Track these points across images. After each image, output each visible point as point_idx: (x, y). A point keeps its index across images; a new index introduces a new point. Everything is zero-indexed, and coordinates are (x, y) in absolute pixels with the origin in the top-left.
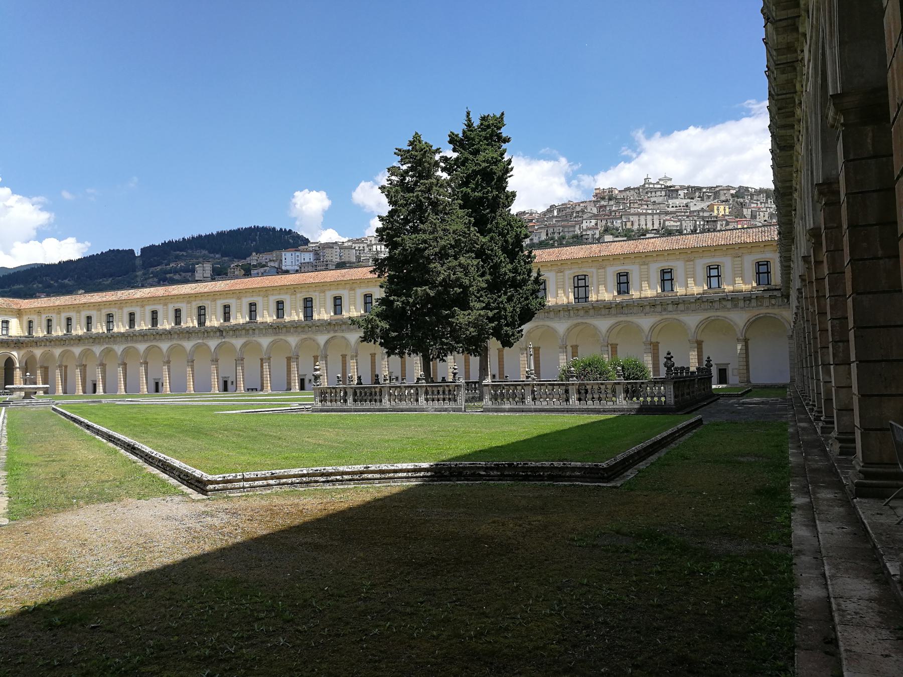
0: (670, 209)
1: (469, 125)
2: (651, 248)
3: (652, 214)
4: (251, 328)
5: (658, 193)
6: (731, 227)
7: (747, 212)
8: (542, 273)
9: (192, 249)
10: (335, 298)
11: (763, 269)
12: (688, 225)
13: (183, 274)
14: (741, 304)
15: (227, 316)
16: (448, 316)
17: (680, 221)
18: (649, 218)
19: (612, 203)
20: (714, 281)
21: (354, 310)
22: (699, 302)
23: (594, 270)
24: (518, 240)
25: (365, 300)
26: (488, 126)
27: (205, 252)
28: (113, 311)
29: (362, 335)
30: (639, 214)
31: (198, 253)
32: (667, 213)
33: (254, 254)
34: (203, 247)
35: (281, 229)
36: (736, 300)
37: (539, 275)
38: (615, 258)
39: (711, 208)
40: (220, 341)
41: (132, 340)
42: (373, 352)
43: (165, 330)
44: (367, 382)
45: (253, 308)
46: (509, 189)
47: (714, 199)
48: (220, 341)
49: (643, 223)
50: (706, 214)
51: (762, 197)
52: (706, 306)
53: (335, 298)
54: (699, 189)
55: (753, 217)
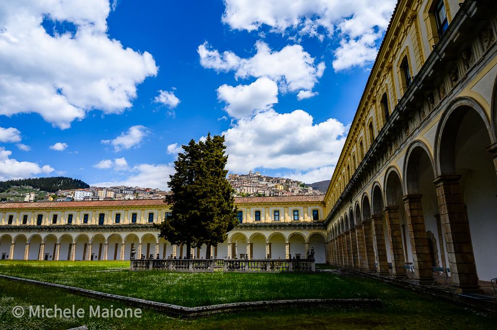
0: (260, 186)
1: (209, 139)
2: (270, 201)
3: (253, 187)
4: (69, 227)
5: (255, 178)
6: (284, 195)
7: (290, 189)
8: (238, 207)
9: (24, 185)
10: (133, 214)
11: (316, 213)
12: (267, 193)
13: (16, 198)
14: (307, 228)
15: (86, 220)
16: (205, 225)
17: (264, 191)
18: (252, 188)
19: (236, 181)
20: (277, 217)
21: (159, 220)
22: (290, 226)
23: (245, 209)
24: (229, 192)
25: (149, 216)
26: (218, 141)
27: (31, 187)
28: (259, 208)
29: (160, 233)
30: (247, 187)
31: (27, 187)
32: (259, 187)
33: (60, 190)
34: (30, 185)
35: (75, 179)
36: (304, 226)
37: (236, 208)
38: (255, 204)
39: (276, 187)
40: (273, 232)
41: (9, 230)
42: (132, 243)
43: (16, 226)
44: (178, 258)
45: (134, 216)
46: (225, 169)
47: (277, 183)
48: (273, 232)
49: (249, 190)
50: (274, 189)
51: (296, 184)
52: (145, 229)
53: (133, 214)
54: (272, 178)
55: (293, 192)
